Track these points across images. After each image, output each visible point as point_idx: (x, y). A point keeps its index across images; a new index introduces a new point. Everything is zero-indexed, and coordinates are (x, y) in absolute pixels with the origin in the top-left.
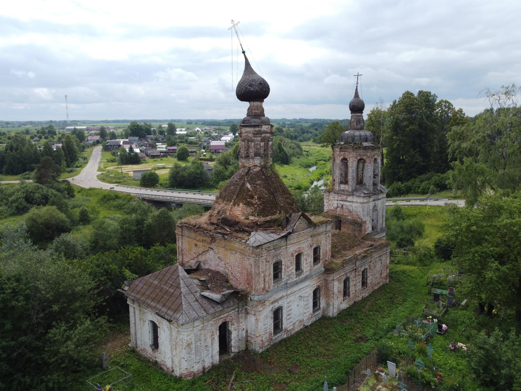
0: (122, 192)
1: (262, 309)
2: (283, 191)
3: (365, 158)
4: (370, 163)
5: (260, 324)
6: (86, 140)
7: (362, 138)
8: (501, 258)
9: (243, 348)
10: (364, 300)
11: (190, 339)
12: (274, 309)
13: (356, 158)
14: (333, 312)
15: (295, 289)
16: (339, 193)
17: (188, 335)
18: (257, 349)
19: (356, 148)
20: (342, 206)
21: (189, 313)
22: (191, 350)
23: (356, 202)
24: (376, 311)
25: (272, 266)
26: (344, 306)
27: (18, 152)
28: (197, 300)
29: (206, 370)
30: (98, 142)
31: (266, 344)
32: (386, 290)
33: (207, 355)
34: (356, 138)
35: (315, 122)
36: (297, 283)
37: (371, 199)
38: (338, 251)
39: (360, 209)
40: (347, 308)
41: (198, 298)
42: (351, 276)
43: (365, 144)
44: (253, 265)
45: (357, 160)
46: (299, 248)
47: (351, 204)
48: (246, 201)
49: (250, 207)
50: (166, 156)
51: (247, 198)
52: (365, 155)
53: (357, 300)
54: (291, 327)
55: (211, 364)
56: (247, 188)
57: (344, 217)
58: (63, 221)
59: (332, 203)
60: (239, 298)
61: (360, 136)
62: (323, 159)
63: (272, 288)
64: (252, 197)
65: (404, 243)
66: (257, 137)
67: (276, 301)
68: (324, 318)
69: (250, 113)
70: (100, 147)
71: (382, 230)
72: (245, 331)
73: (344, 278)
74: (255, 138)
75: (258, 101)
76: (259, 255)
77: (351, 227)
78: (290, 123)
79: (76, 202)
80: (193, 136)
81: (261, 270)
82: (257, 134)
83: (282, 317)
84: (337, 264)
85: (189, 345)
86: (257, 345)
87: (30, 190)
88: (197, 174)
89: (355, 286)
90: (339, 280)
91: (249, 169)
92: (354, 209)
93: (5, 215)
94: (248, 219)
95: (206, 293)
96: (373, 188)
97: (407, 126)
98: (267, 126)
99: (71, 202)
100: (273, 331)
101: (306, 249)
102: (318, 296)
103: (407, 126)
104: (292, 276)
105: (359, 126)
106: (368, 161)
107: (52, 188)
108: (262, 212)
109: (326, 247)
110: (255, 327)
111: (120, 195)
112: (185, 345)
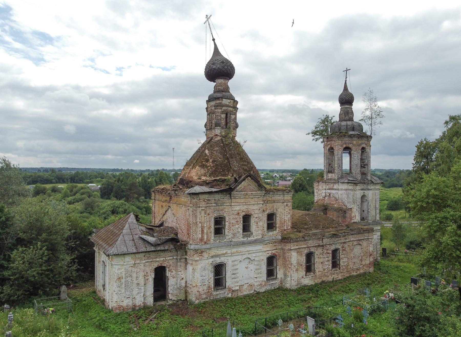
2: (241, 159)
3: (350, 146)
4: (356, 150)
5: (197, 275)
7: (349, 127)
9: (182, 297)
11: (121, 273)
13: (342, 146)
15: (242, 249)
17: (119, 269)
18: (194, 299)
19: (342, 136)
20: (330, 194)
22: (122, 284)
23: (342, 189)
25: (213, 220)
26: (308, 281)
28: (133, 240)
29: (137, 308)
31: (204, 296)
33: (138, 293)
34: (342, 128)
36: (243, 244)
37: (358, 187)
38: (307, 228)
39: (345, 196)
42: (318, 252)
51: (202, 162)
54: (237, 288)
55: (143, 303)
57: (331, 206)
61: (347, 126)
64: (207, 161)
65: (414, 246)
66: (218, 109)
69: (217, 90)
72: (183, 282)
73: (306, 251)
74: (216, 110)
75: (221, 78)
81: (198, 220)
82: (217, 106)
83: (225, 274)
85: (119, 278)
86: (194, 296)
87: (116, 206)
89: (322, 263)
90: (298, 251)
94: (200, 179)
96: (362, 177)
98: (228, 100)
100: (213, 285)
101: (257, 212)
106: (353, 148)
110: (192, 277)
112: (116, 278)
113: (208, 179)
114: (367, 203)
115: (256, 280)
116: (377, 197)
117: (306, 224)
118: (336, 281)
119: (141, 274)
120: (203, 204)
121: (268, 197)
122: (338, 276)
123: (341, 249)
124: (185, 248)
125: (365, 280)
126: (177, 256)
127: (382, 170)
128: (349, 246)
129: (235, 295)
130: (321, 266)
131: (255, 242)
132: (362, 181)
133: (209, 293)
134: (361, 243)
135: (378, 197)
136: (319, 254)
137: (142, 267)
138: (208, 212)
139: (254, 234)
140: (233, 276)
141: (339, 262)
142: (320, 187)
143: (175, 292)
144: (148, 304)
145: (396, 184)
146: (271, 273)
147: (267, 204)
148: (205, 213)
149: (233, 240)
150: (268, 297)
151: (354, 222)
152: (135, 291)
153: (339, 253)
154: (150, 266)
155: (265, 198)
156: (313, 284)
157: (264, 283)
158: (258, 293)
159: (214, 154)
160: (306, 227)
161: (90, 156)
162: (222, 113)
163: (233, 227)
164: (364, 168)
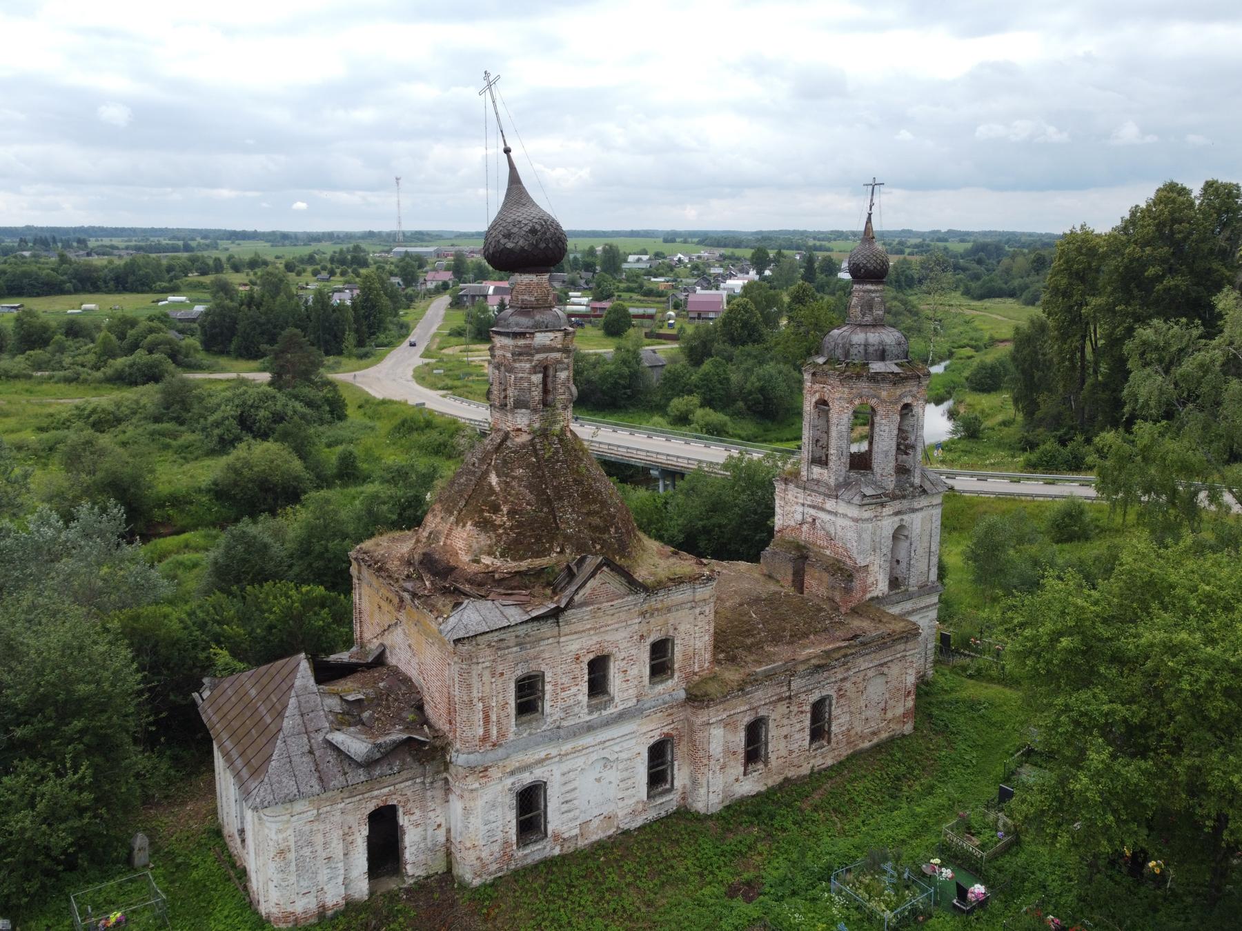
0: (443, 414)
1: (476, 785)
2: (585, 496)
4: (887, 416)
5: (476, 822)
6: (421, 280)
7: (871, 349)
8: (1132, 739)
9: (440, 867)
10: (817, 776)
11: (286, 840)
12: (518, 787)
13: (851, 402)
14: (708, 799)
15: (588, 740)
16: (808, 486)
17: (279, 831)
18: (468, 877)
19: (850, 377)
21: (280, 782)
22: (288, 864)
23: (845, 516)
24: (835, 810)
25: (513, 686)
26: (749, 786)
27: (262, 309)
29: (329, 913)
30: (444, 287)
31: (494, 867)
32: (892, 755)
33: (330, 879)
34: (853, 351)
35: (981, 240)
36: (590, 728)
37: (887, 510)
39: (851, 535)
40: (759, 794)
41: (315, 747)
42: (775, 715)
43: (877, 367)
44: (456, 679)
46: (598, 643)
47: (833, 518)
48: (481, 516)
50: (581, 325)
51: (483, 511)
53: (792, 773)
54: (576, 831)
57: (816, 549)
58: (297, 478)
59: (793, 509)
60: (425, 751)
61: (866, 345)
62: (973, 343)
63: (511, 737)
64: (496, 509)
67: (526, 768)
70: (446, 299)
71: (925, 589)
72: (443, 831)
73: (747, 719)
74: (517, 365)
75: (529, 272)
76: (471, 658)
77: (826, 577)
78: (918, 241)
79: (342, 432)
80: (661, 275)
81: (475, 694)
82: (520, 354)
83: (546, 806)
84: (724, 683)
86: (468, 869)
87: (250, 403)
88: (621, 376)
89: (789, 744)
90: (728, 724)
91: (506, 436)
92: (840, 533)
93: (196, 454)
94: (477, 561)
95: (338, 738)
97: (1159, 278)
99: (321, 433)
100: (514, 838)
102: (669, 758)
103: (1159, 278)
104: (576, 709)
105: (868, 319)
106: (881, 410)
107: (296, 397)
108: (512, 550)
109: (694, 638)
110: (464, 826)
111: (437, 421)
113: (498, 563)
114: (907, 544)
115: (621, 804)
117: (749, 633)
118: (819, 773)
119: (336, 835)
120: (486, 657)
121: (655, 602)
122: (825, 758)
123: (835, 696)
124: (444, 756)
125: (889, 765)
126: (424, 776)
127: (968, 234)
128: (854, 683)
129: (569, 848)
130: (783, 743)
131: (622, 717)
132: (897, 492)
133: (506, 856)
134: (885, 670)
135: (937, 523)
136: (778, 717)
137: (338, 818)
138: (500, 669)
141: (830, 727)
142: (790, 496)
143: (422, 857)
144: (357, 896)
145: (1001, 289)
146: (658, 778)
147: (652, 620)
148: (493, 675)
149: (565, 724)
150: (651, 848)
151: (872, 599)
152: (323, 875)
153: (830, 705)
154: (358, 809)
155: (645, 607)
156: (763, 789)
157: (641, 806)
158: (626, 833)
159: (513, 488)
160: (749, 641)
161: (170, 190)
162: (534, 370)
163: (565, 692)
164: (907, 454)
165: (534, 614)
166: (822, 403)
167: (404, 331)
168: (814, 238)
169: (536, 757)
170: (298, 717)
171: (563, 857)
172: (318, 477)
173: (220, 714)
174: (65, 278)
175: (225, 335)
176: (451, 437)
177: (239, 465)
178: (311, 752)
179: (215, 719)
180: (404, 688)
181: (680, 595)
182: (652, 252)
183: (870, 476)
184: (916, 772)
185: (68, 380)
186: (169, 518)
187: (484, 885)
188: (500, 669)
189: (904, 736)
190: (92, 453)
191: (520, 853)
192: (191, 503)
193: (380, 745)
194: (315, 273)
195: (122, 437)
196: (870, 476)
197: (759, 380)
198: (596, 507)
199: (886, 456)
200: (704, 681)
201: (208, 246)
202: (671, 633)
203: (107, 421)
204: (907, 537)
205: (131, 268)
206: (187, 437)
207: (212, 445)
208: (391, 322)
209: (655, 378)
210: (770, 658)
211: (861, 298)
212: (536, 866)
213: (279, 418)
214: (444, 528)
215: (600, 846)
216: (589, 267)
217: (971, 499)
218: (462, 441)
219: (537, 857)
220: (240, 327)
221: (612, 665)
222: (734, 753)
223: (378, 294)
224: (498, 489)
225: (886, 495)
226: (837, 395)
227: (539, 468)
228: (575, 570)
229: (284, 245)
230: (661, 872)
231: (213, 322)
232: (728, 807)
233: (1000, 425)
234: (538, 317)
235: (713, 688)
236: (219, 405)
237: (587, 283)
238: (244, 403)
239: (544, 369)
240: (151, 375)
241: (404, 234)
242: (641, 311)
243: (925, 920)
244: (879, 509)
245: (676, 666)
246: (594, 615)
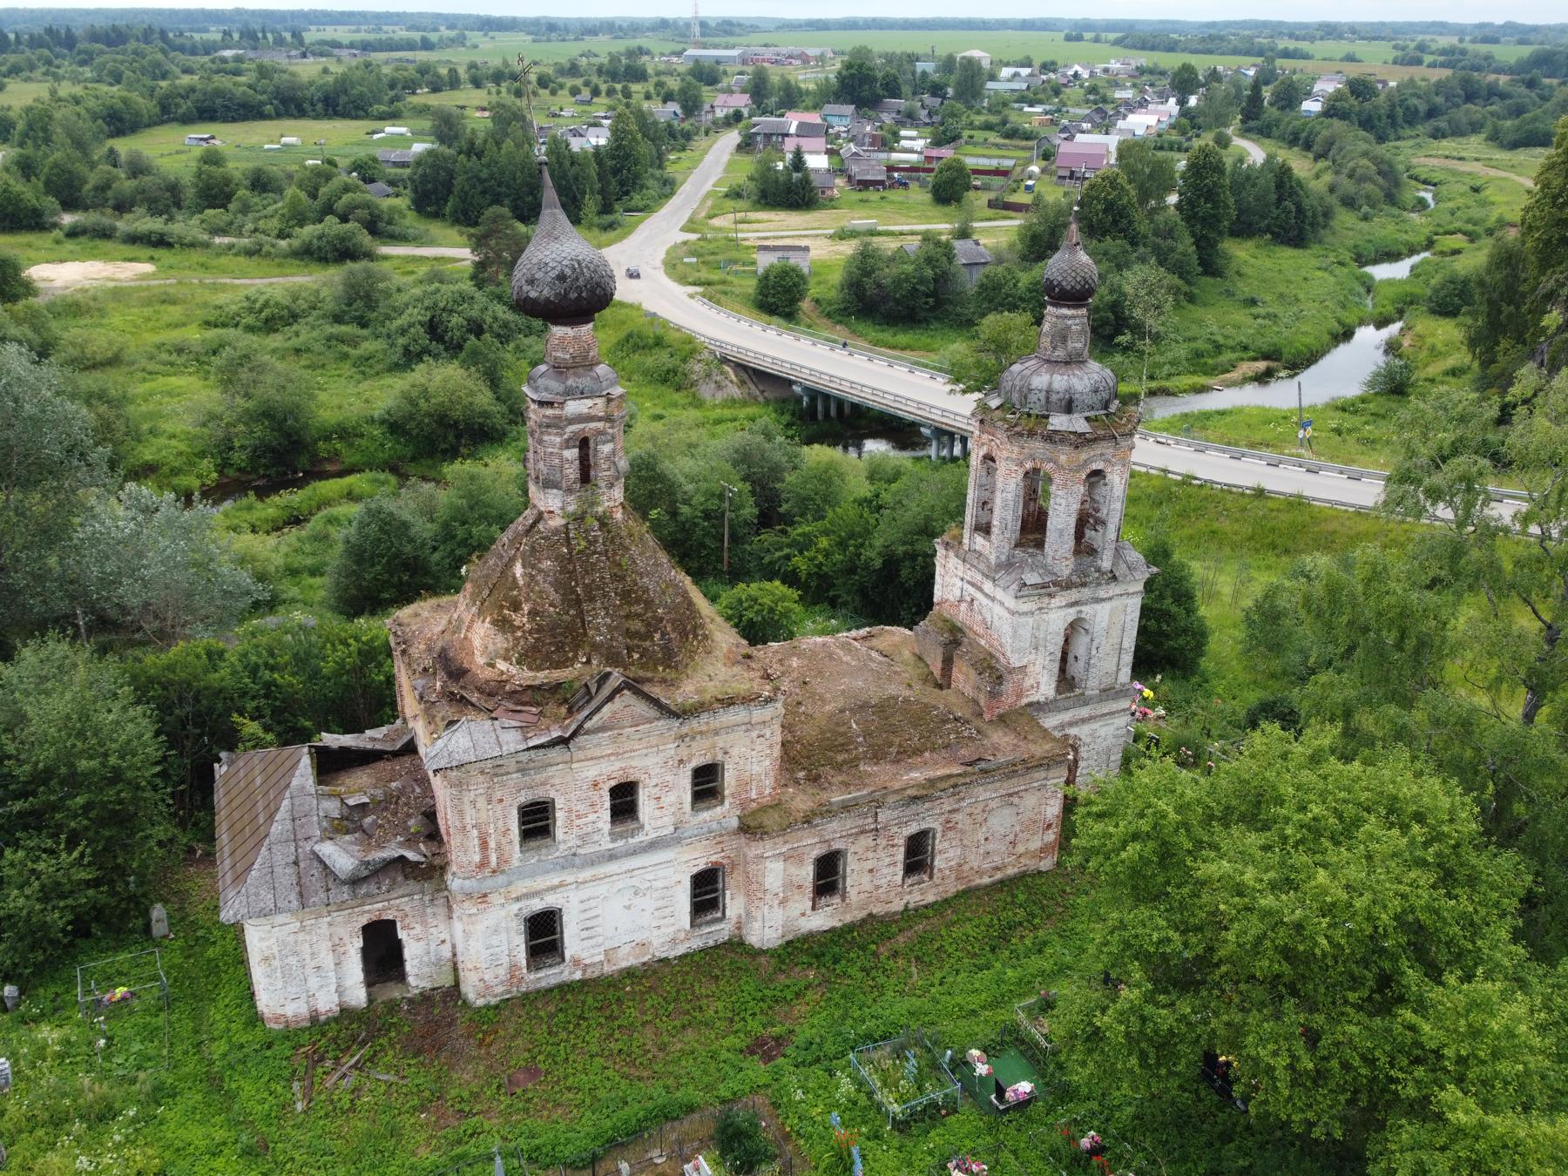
0: (679, 329)
1: (474, 911)
4: (1065, 486)
6: (707, 107)
7: (1054, 398)
8: (1178, 977)
9: (447, 981)
10: (910, 915)
12: (527, 913)
13: (1021, 464)
17: (262, 939)
18: (471, 996)
19: (1020, 435)
21: (257, 894)
23: (1002, 604)
26: (822, 920)
27: (484, 160)
29: (323, 1018)
30: (737, 117)
31: (500, 989)
32: (1014, 896)
34: (1032, 398)
36: (612, 857)
40: (832, 930)
41: (301, 857)
43: (1058, 422)
45: (1021, 472)
48: (500, 613)
49: (504, 633)
51: (502, 607)
52: (1050, 460)
53: (877, 909)
56: (514, 577)
57: (972, 635)
58: (485, 415)
62: (1470, 227)
63: (515, 863)
64: (516, 607)
68: (736, 945)
70: (733, 137)
72: (448, 946)
73: (817, 852)
75: (565, 324)
77: (973, 674)
78: (1454, 40)
80: (1040, 102)
82: (548, 426)
87: (441, 305)
88: (922, 281)
94: (492, 666)
95: (327, 849)
100: (524, 962)
105: (1060, 354)
108: (530, 657)
109: (751, 759)
110: (463, 941)
111: (672, 336)
114: (1086, 639)
115: (656, 932)
116: (1129, 618)
117: (843, 748)
118: (916, 910)
122: (924, 893)
123: (939, 829)
125: (1016, 906)
130: (866, 878)
131: (653, 846)
132: (1074, 579)
139: (647, 827)
140: (585, 934)
143: (426, 970)
144: (353, 1003)
147: (694, 744)
148: (489, 802)
151: (1030, 705)
152: (313, 982)
153: (934, 838)
156: (839, 924)
157: (682, 935)
159: (537, 583)
160: (840, 758)
162: (567, 445)
165: (531, 744)
166: (989, 458)
167: (667, 189)
168: (1291, 36)
169: (548, 884)
170: (288, 822)
171: (583, 983)
172: (511, 411)
173: (229, 797)
174: (264, 98)
175: (440, 193)
176: (684, 360)
177: (414, 394)
178: (296, 863)
179: (223, 803)
180: (418, 790)
181: (736, 715)
182: (1037, 63)
183: (1040, 558)
184: (1036, 921)
185: (249, 253)
186: (337, 453)
187: (488, 1007)
188: (499, 795)
189: (1040, 872)
190: (251, 370)
191: (532, 976)
192: (362, 436)
193: (368, 863)
194: (575, 92)
195: (295, 342)
196: (1040, 558)
197: (1111, 292)
198: (638, 609)
199: (1061, 535)
200: (764, 809)
201: (452, 40)
202: (720, 757)
203: (281, 318)
204: (1087, 631)
205: (343, 85)
206: (369, 346)
207: (395, 358)
208: (652, 175)
209: (970, 283)
210: (861, 780)
211: (1054, 325)
212: (551, 990)
213: (477, 329)
214: (467, 617)
215: (629, 973)
216: (937, 90)
217: (1321, 510)
218: (697, 368)
219: (553, 981)
220: (459, 181)
221: (641, 791)
222: (800, 887)
223: (634, 139)
224: (521, 583)
225: (1055, 584)
226: (1005, 454)
227: (570, 560)
228: (593, 691)
229: (549, 40)
230: (687, 1013)
231: (424, 175)
232: (789, 943)
233: (1447, 373)
234: (570, 382)
235: (771, 820)
236: (407, 305)
237: (930, 115)
238: (435, 304)
239: (584, 444)
240: (344, 252)
241: (703, 24)
242: (993, 163)
243: (948, 1114)
244: (1046, 600)
245: (727, 792)
246: (614, 740)
